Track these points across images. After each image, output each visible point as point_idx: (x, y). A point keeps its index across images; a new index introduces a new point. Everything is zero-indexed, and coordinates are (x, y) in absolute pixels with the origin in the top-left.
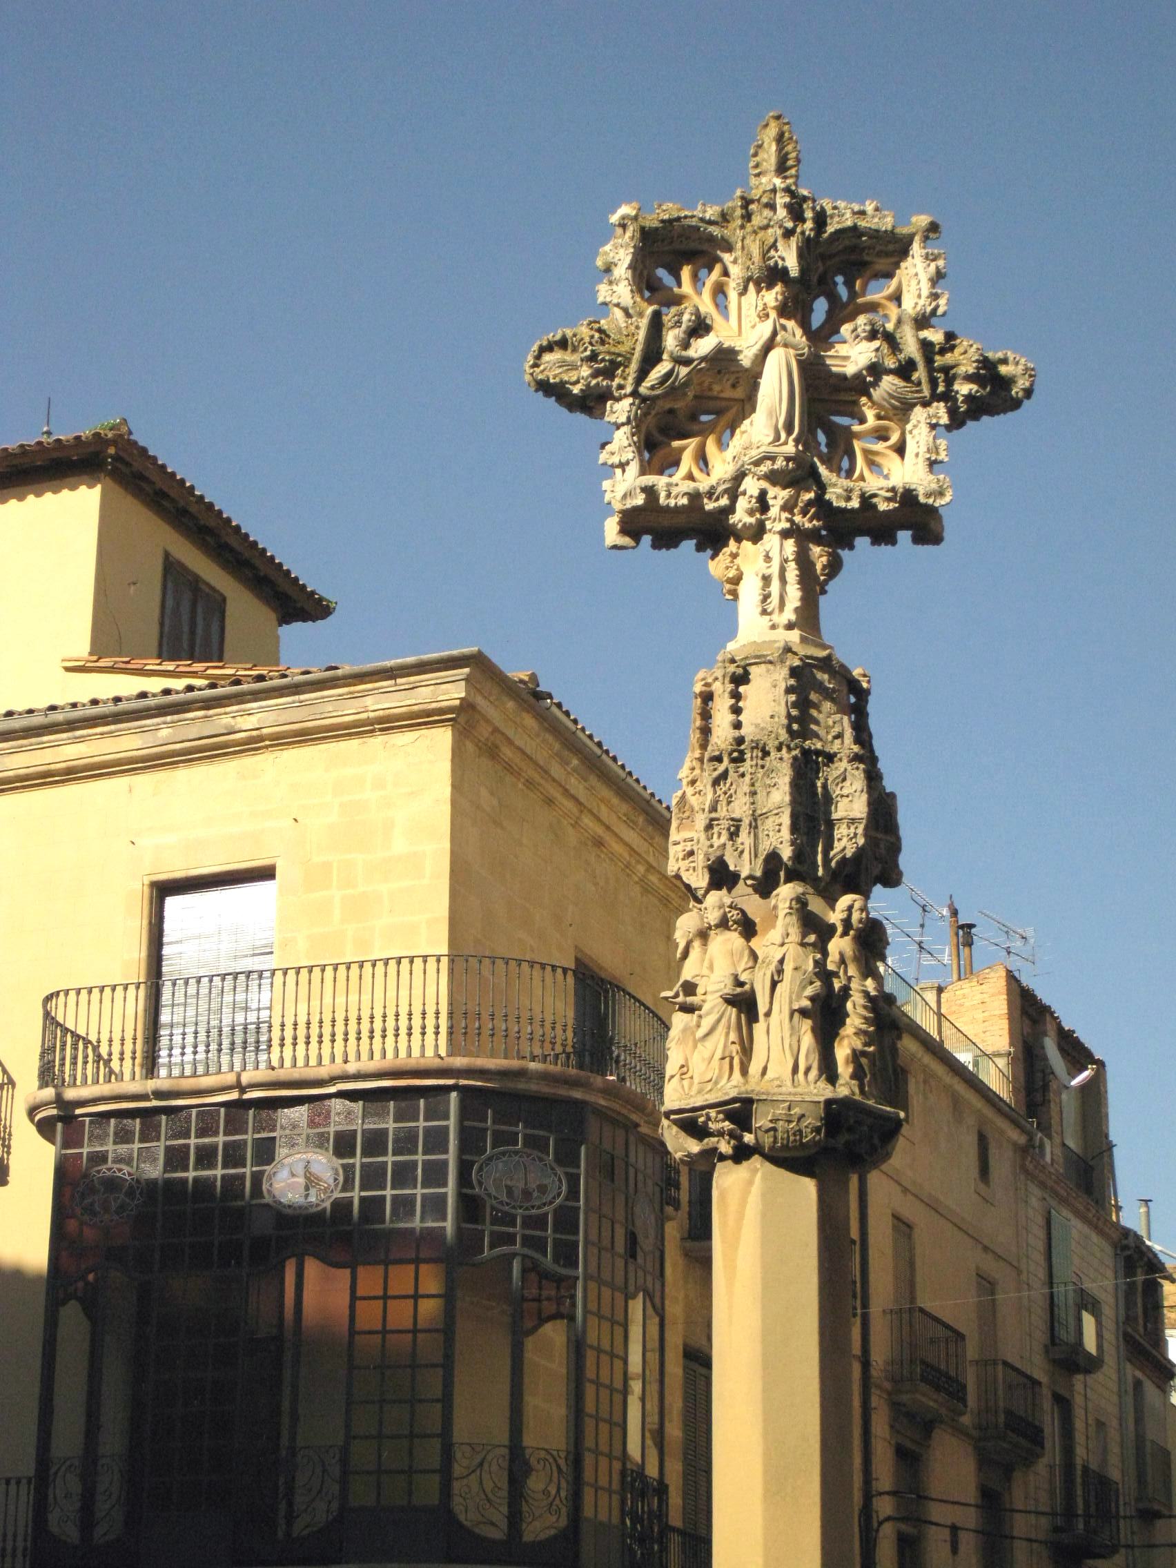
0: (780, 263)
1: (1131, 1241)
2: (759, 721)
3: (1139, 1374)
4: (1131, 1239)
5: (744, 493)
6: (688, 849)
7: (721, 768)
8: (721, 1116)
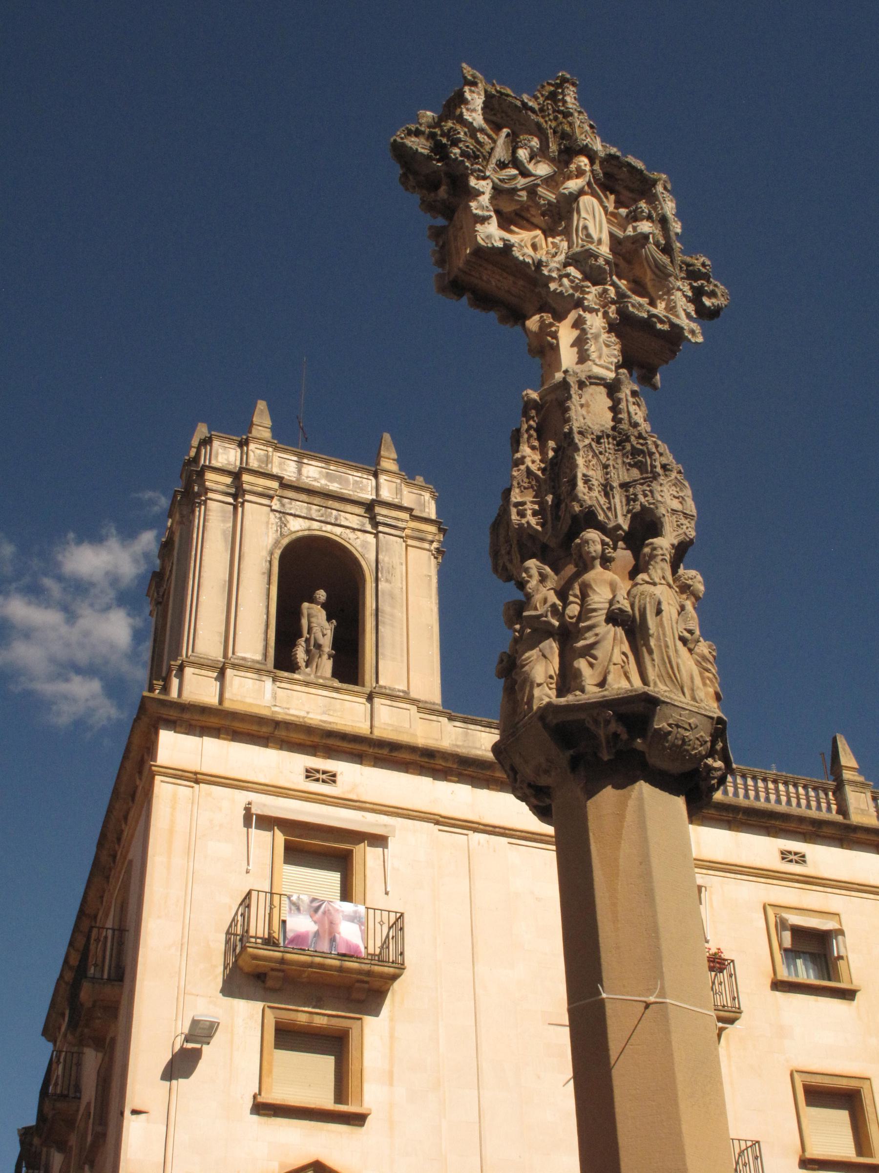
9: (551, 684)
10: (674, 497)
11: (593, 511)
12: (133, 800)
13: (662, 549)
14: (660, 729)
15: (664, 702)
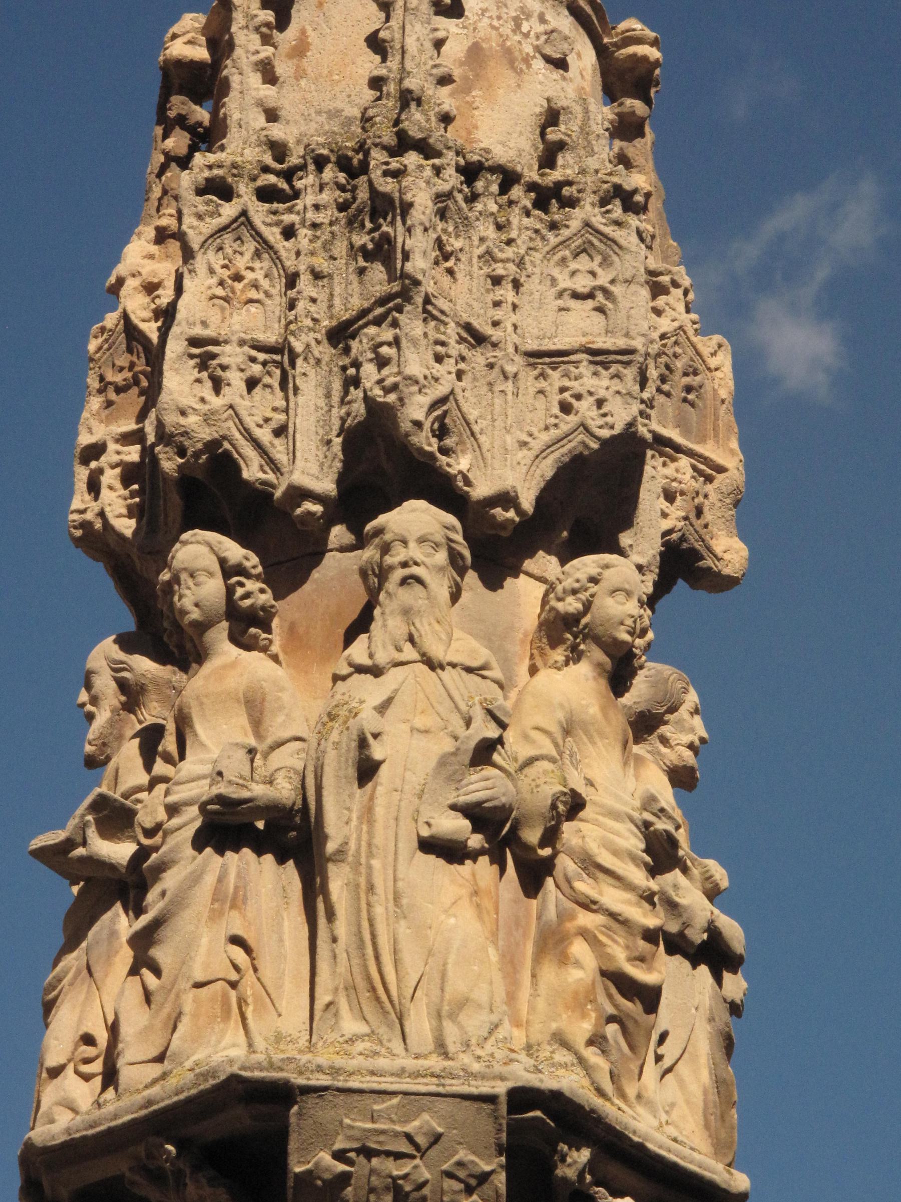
7: (229, 210)
9: (87, 1061)
10: (576, 296)
11: (227, 454)
12: (611, 1073)
13: (405, 542)
14: (309, 1172)
15: (307, 1090)
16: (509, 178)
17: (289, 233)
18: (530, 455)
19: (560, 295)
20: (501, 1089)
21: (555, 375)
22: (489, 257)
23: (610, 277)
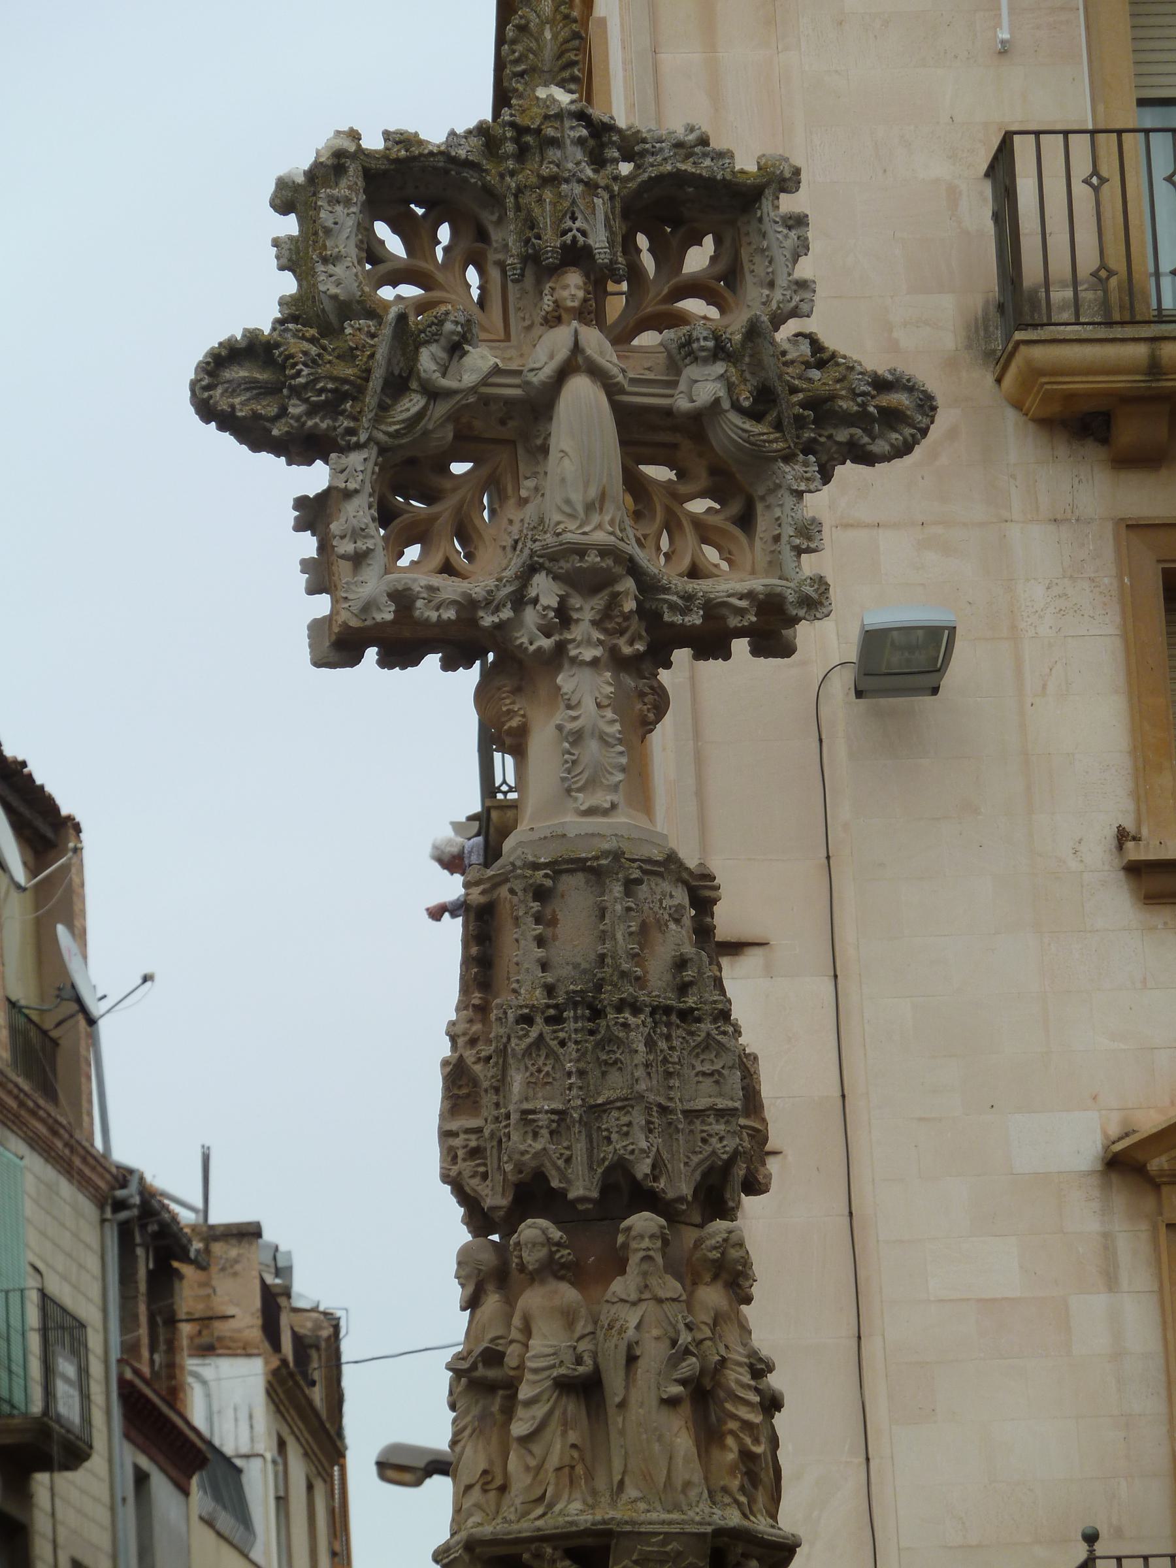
0: (581, 239)
1: (131, 1193)
2: (579, 960)
3: (144, 1463)
4: (133, 1188)
5: (535, 601)
6: (473, 1144)
7: (534, 1033)
8: (558, 1554)
10: (704, 1074)
16: (668, 1010)
17: (563, 1044)
18: (690, 1169)
19: (697, 1075)
20: (709, 1529)
21: (698, 1122)
22: (665, 1061)
23: (721, 1065)
